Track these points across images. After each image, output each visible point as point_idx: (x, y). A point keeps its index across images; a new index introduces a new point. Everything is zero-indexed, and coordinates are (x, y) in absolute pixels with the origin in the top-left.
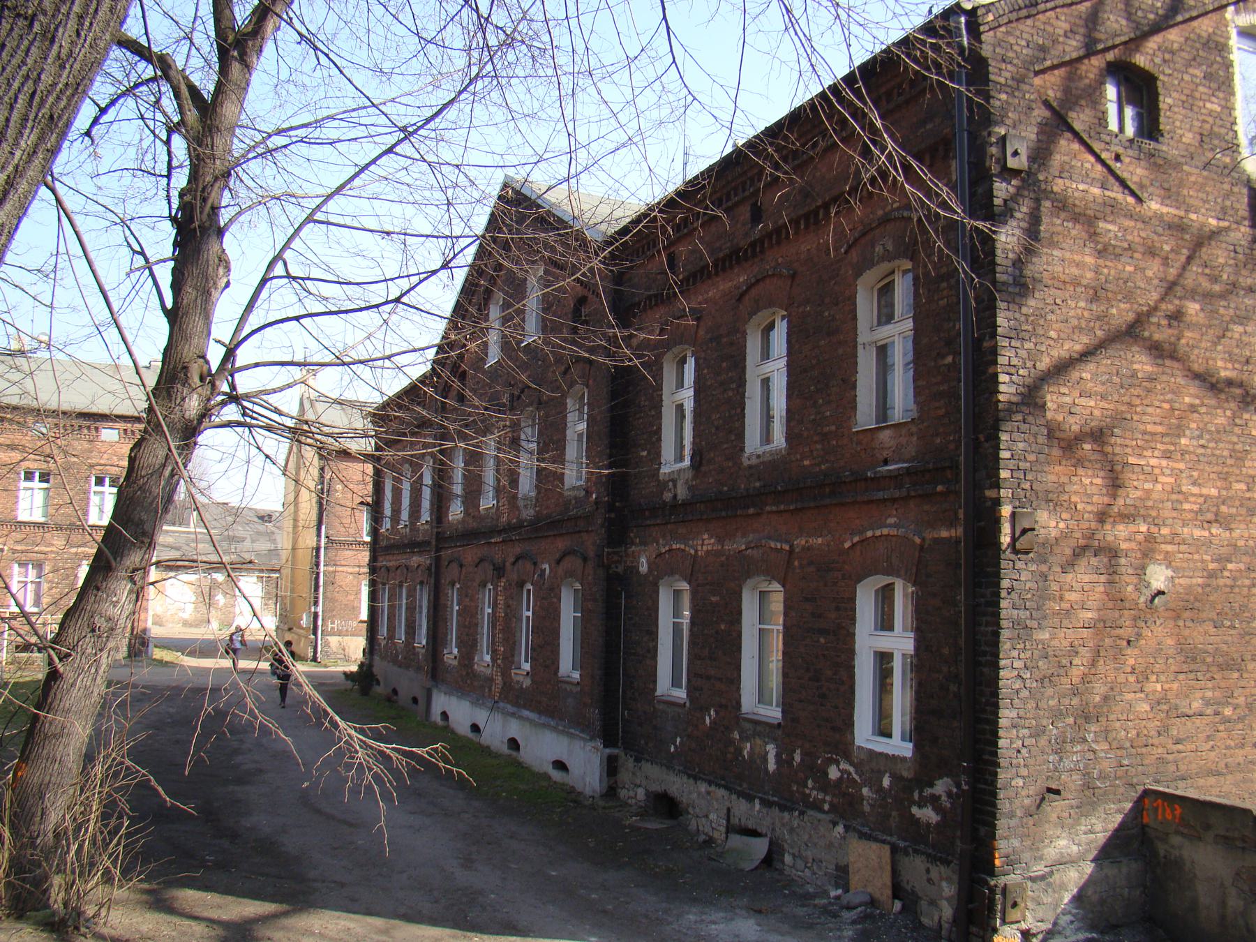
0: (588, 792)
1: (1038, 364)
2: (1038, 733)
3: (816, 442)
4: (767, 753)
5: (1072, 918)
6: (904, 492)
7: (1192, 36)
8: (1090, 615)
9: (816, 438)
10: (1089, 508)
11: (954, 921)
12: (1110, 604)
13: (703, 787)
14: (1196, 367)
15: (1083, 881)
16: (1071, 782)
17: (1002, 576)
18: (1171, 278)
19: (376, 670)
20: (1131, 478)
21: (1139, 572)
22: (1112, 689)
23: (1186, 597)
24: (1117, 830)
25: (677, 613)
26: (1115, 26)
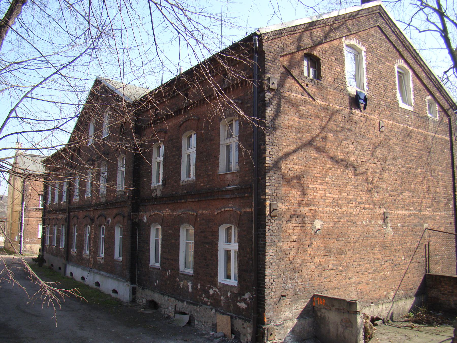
0: (125, 301)
1: (279, 154)
2: (279, 277)
3: (205, 178)
4: (188, 285)
5: (290, 338)
6: (235, 196)
7: (332, 46)
8: (296, 237)
9: (205, 176)
10: (296, 202)
11: (252, 340)
12: (302, 234)
13: (166, 298)
14: (331, 155)
15: (294, 325)
16: (289, 293)
17: (266, 225)
18: (323, 125)
19: (45, 257)
20: (310, 192)
21: (312, 223)
22: (303, 261)
23: (327, 231)
24: (305, 308)
25: (157, 236)
26: (307, 42)
